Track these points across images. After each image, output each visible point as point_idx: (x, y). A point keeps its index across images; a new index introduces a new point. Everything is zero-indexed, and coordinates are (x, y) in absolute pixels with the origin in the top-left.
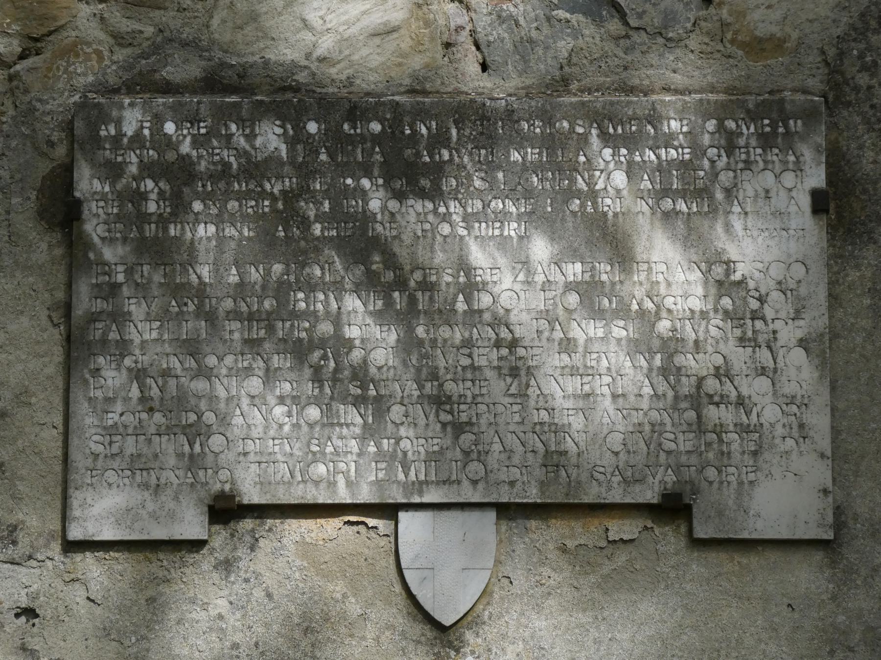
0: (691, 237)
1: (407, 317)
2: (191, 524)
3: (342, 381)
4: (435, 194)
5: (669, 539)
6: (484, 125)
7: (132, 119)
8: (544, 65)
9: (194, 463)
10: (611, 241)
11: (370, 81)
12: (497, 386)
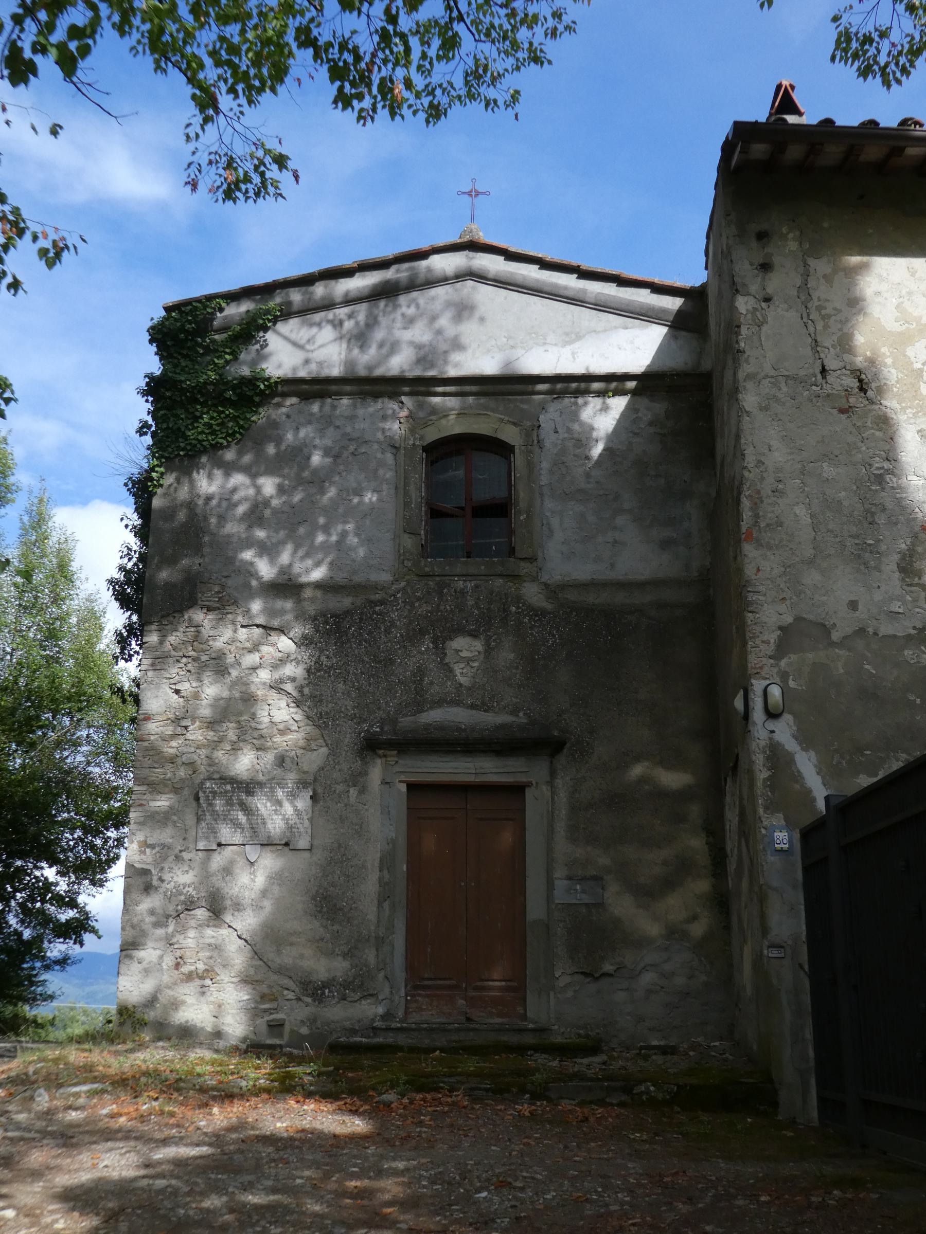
0: (292, 803)
1: (248, 815)
2: (214, 847)
3: (237, 825)
4: (253, 796)
5: (286, 849)
6: (261, 785)
7: (208, 784)
8: (272, 775)
9: (215, 837)
10: (279, 803)
11: (245, 778)
12: (261, 826)
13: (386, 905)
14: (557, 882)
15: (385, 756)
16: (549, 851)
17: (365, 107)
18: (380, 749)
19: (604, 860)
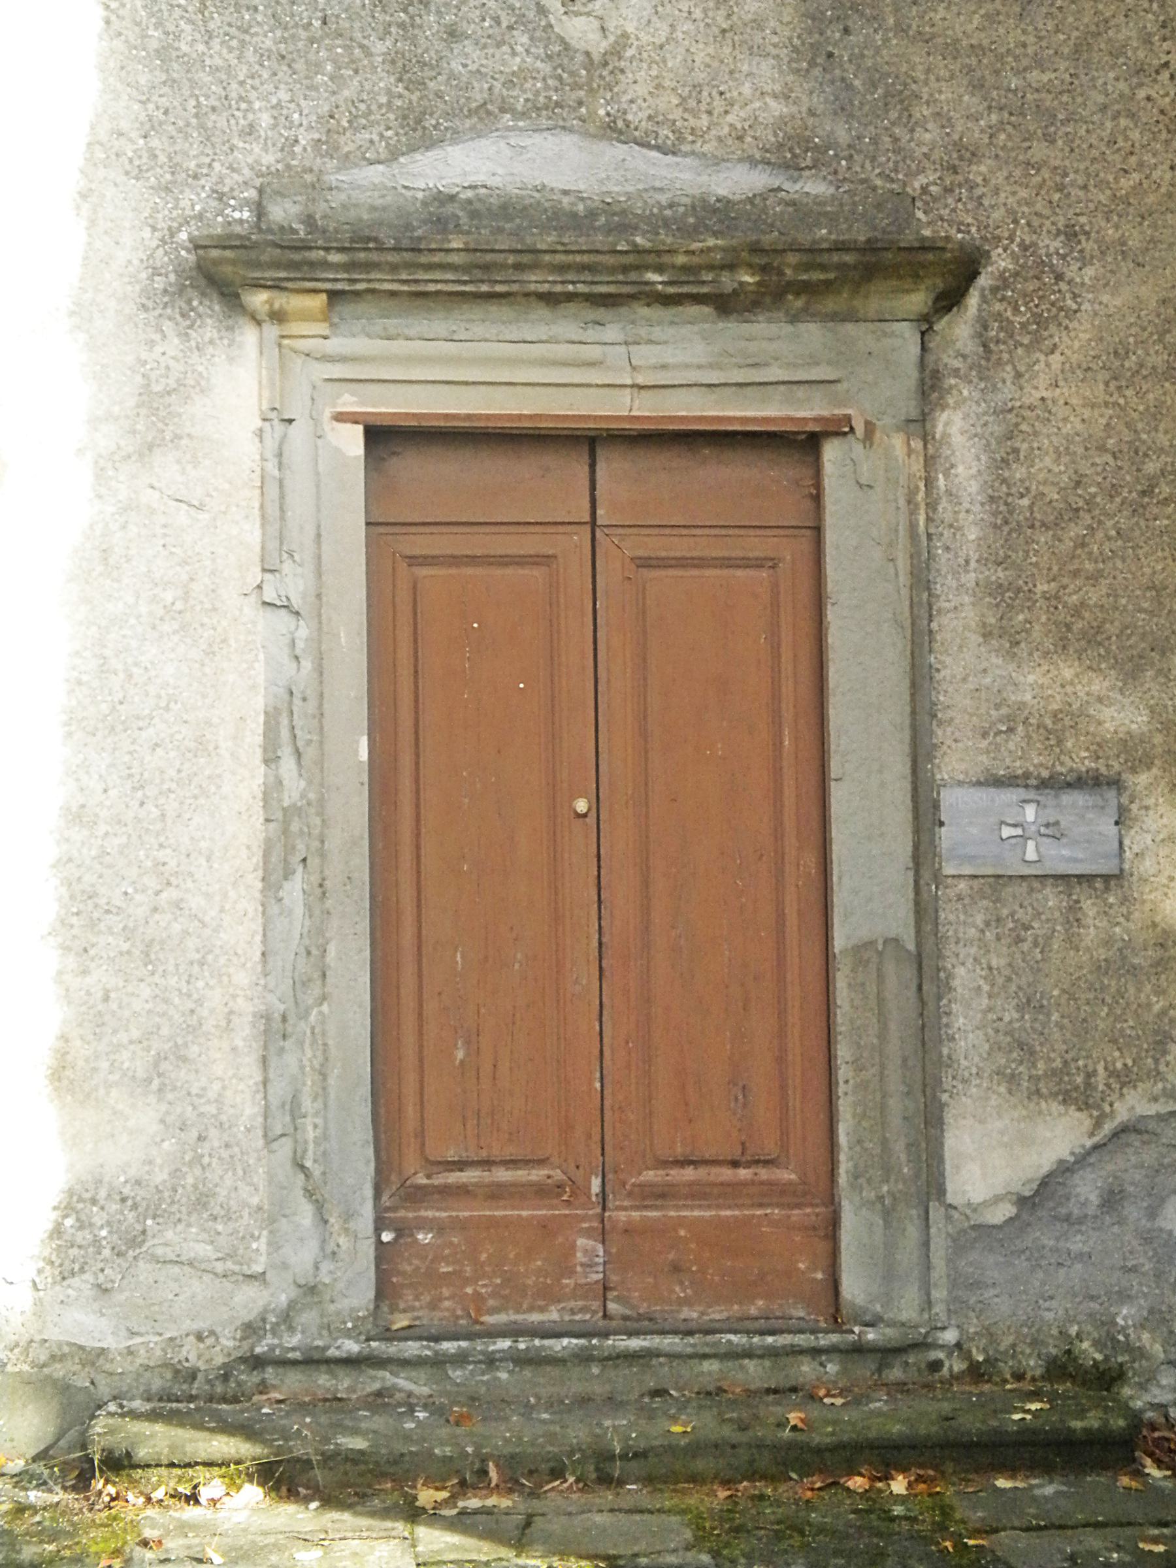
13: (294, 890)
14: (950, 799)
15: (278, 317)
16: (920, 679)
17: (287, 885)
18: (258, 285)
19: (1122, 715)
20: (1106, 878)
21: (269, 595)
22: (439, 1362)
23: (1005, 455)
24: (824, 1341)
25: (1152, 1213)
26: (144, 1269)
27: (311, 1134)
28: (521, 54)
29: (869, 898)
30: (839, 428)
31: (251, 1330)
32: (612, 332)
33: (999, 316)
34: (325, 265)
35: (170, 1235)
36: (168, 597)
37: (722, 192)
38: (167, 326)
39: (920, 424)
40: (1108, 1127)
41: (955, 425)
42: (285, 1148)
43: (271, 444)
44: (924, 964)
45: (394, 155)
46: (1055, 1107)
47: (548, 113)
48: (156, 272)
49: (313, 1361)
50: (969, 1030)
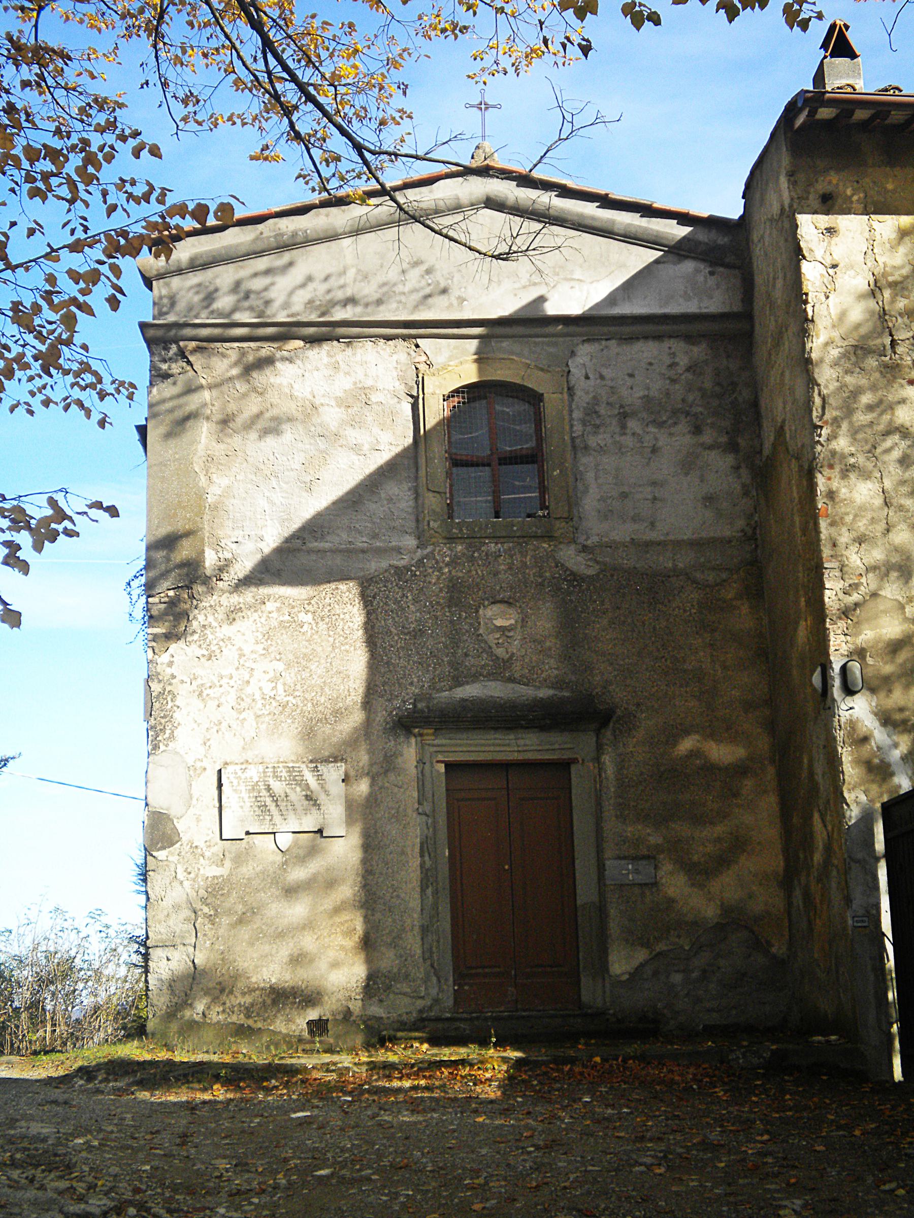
13: (429, 891)
14: (608, 863)
15: (421, 735)
20: (652, 884)
21: (420, 810)
22: (471, 1019)
23: (621, 767)
24: (576, 1013)
25: (667, 977)
26: (392, 996)
27: (436, 958)
28: (484, 660)
29: (586, 892)
30: (574, 761)
31: (421, 1011)
32: (512, 737)
33: (619, 728)
34: (433, 721)
35: (398, 986)
36: (393, 812)
37: (541, 696)
38: (391, 738)
39: (597, 759)
40: (654, 953)
41: (607, 759)
42: (429, 962)
43: (420, 769)
44: (601, 910)
45: (451, 689)
46: (639, 948)
47: (492, 676)
48: (387, 723)
49: (438, 1019)
50: (614, 928)
